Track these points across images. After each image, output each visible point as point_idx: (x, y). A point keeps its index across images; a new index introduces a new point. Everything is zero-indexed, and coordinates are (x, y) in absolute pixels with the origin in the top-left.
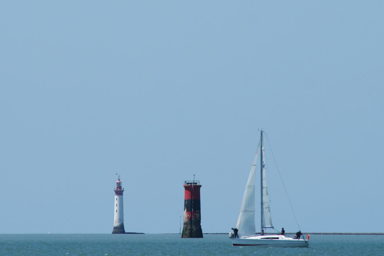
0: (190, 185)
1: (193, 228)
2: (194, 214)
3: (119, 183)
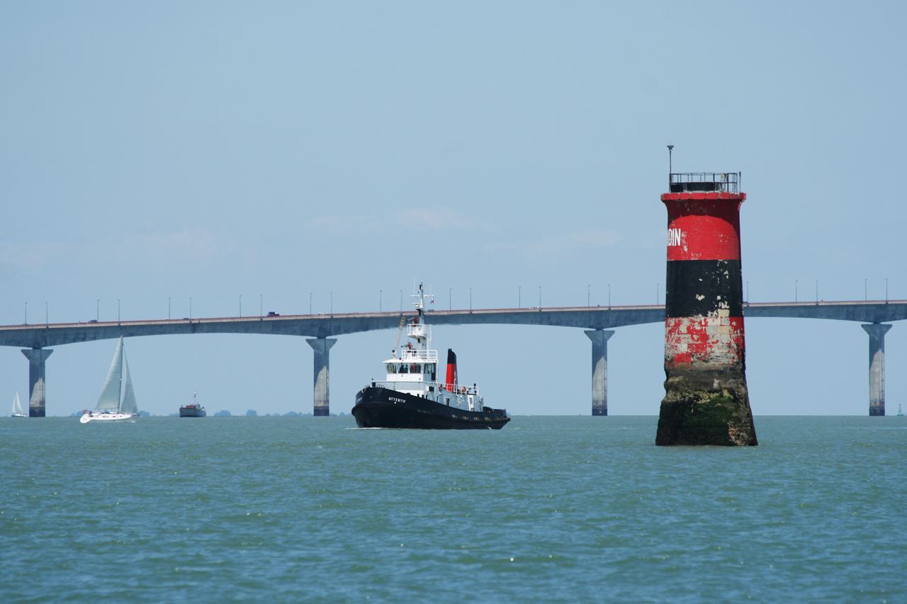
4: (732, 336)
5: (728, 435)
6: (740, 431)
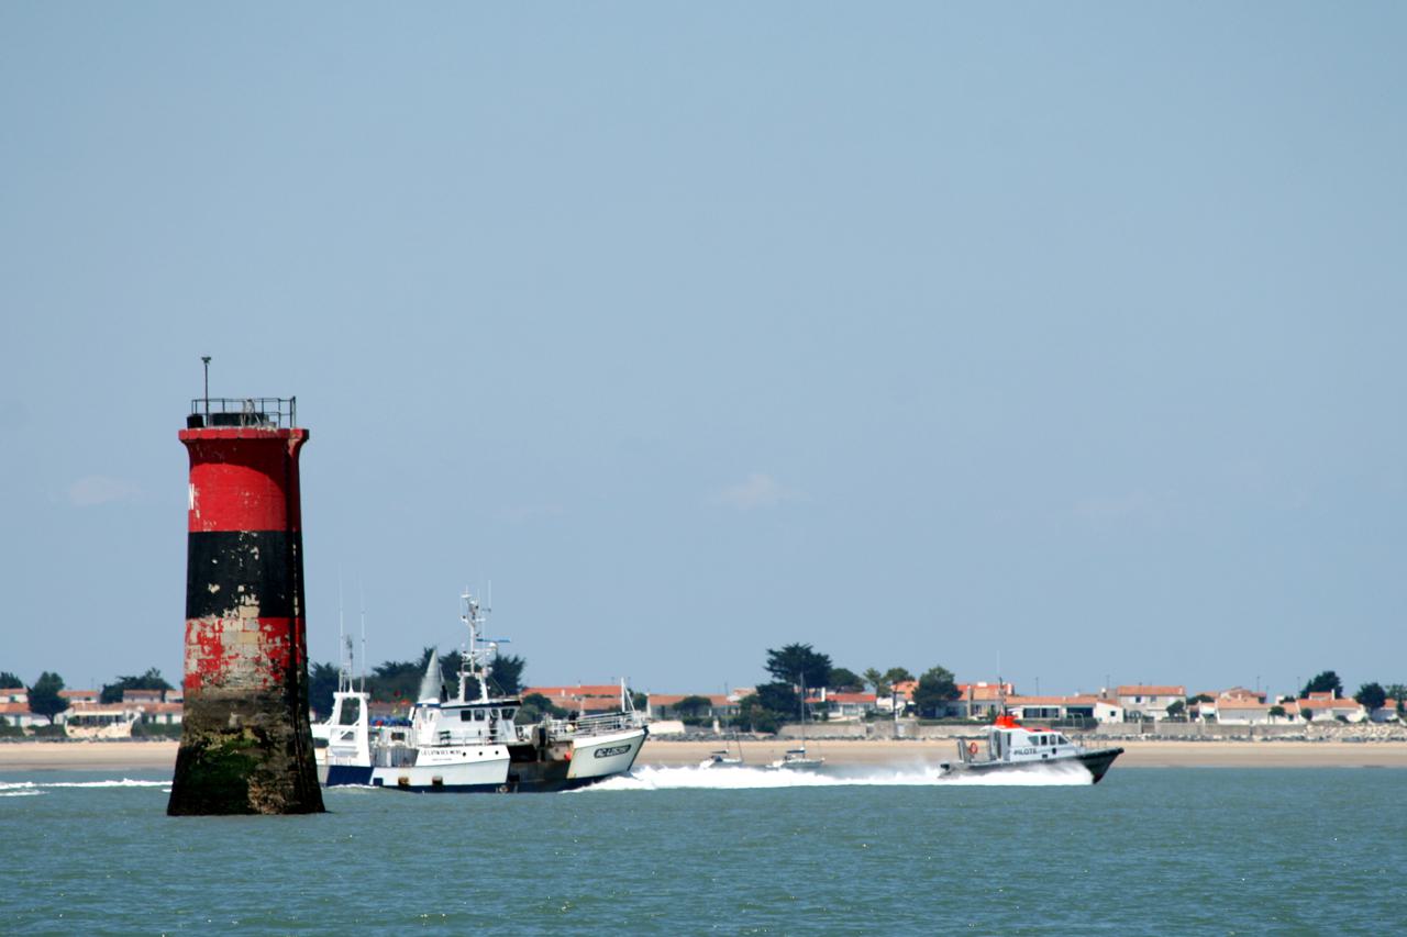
4: (264, 647)
5: (247, 798)
6: (270, 792)
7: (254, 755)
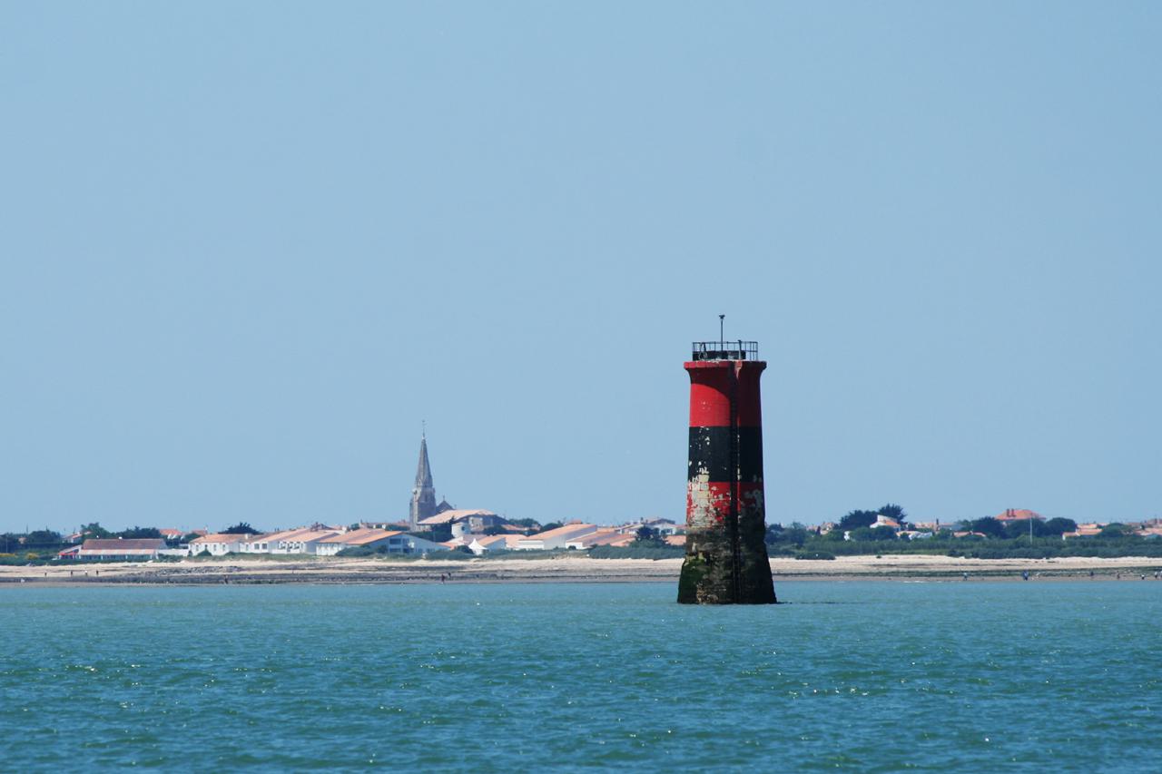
0: (718, 360)
1: (736, 559)
2: (747, 494)
3: (387, 550)
4: (712, 500)
5: (695, 597)
6: (708, 593)
7: (701, 569)
